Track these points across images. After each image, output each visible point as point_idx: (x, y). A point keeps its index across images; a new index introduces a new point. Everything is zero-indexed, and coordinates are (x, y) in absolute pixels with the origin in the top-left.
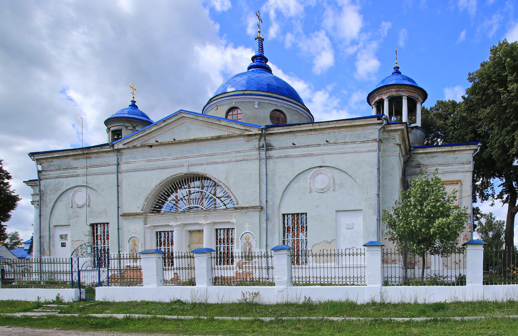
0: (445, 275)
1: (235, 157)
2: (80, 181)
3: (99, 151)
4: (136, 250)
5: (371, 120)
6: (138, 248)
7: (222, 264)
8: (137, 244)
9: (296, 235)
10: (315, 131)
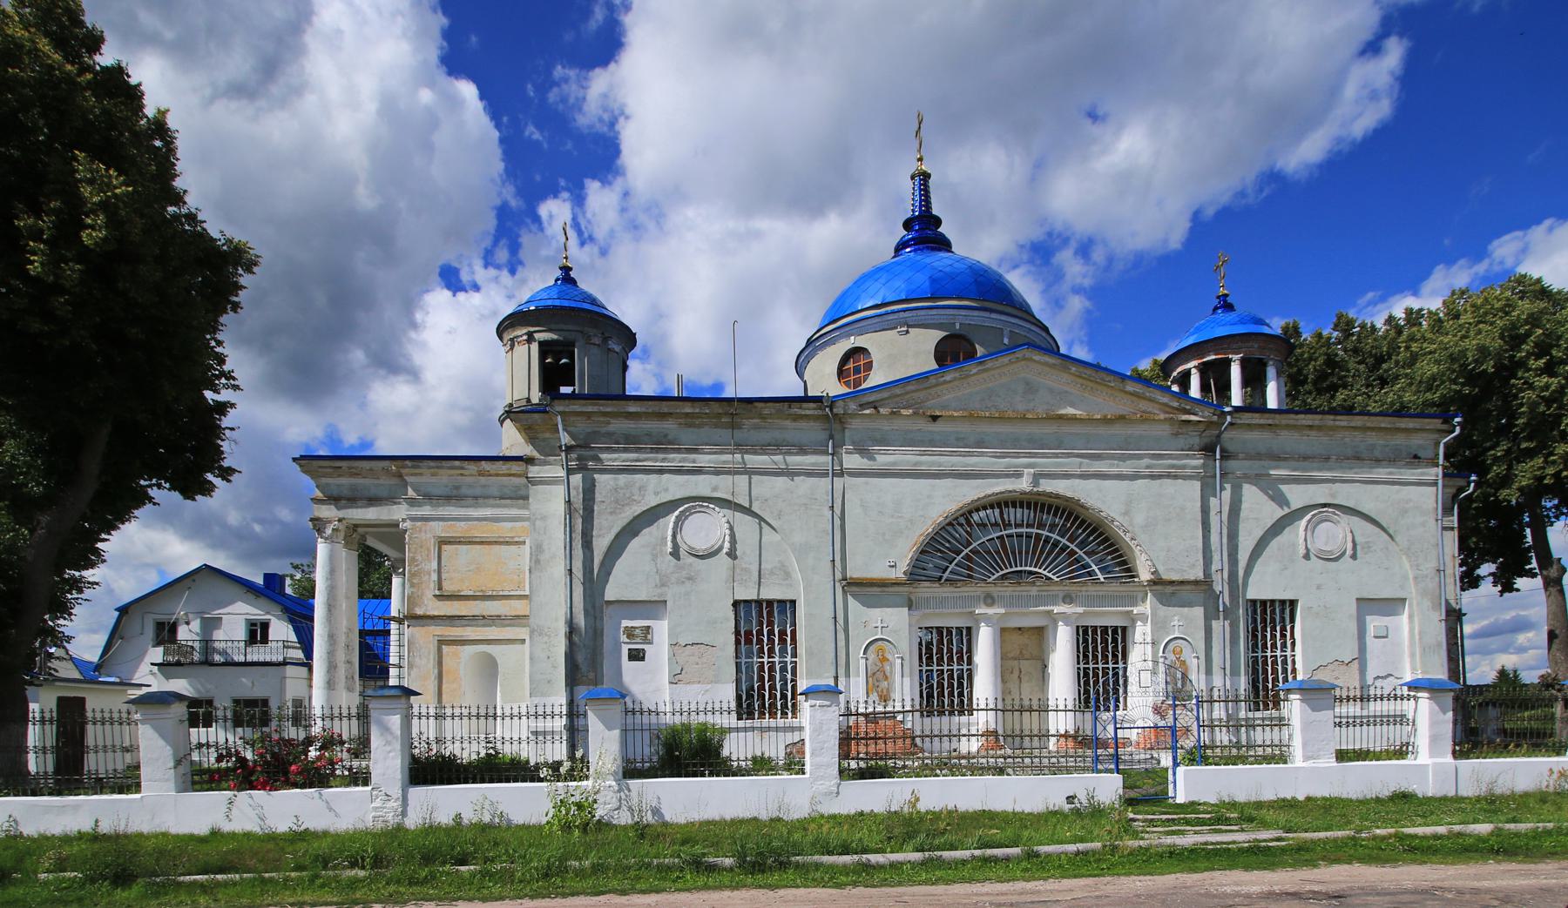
1: (1147, 467)
4: (888, 674)
6: (891, 667)
7: (790, 715)
8: (890, 657)
9: (1269, 646)
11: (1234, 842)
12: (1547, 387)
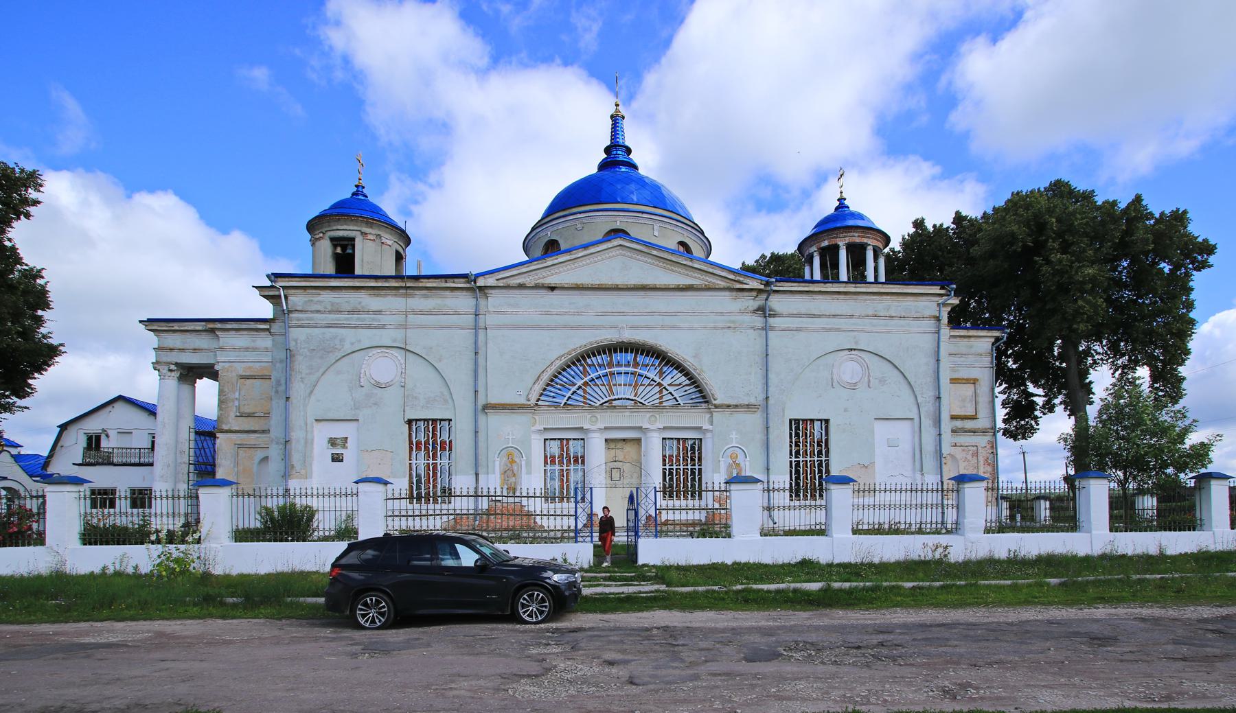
0: (897, 521)
2: (386, 337)
3: (439, 286)
4: (516, 472)
5: (931, 289)
8: (517, 460)
9: (808, 453)
10: (845, 295)
11: (623, 593)
12: (1060, 261)
